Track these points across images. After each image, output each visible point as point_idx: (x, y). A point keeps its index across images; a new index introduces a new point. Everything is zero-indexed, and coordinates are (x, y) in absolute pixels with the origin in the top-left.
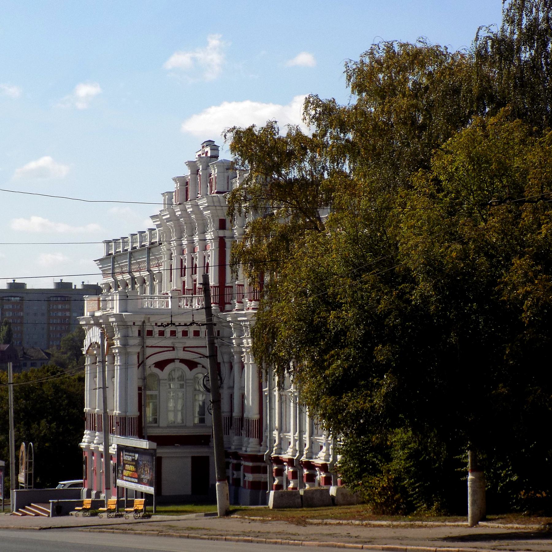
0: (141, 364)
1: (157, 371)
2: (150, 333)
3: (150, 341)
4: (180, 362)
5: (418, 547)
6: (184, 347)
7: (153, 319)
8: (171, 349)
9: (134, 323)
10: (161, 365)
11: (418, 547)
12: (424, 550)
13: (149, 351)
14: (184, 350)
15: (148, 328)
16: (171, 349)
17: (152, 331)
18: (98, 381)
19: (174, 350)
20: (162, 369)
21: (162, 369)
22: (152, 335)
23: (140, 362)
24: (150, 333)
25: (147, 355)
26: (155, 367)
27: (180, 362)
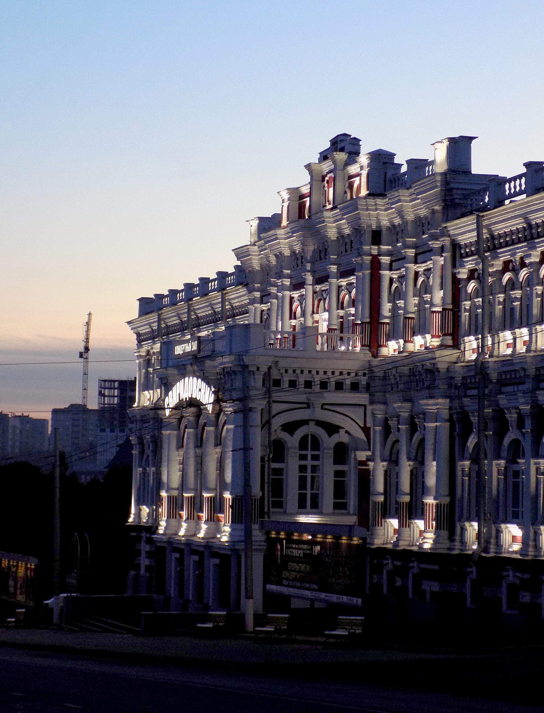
0: (266, 424)
1: (284, 436)
2: (277, 383)
3: (276, 395)
4: (316, 424)
5: (191, 582)
6: (323, 405)
7: (283, 363)
8: (325, 407)
9: (258, 368)
10: (290, 428)
11: (191, 582)
12: (280, 614)
13: (276, 408)
14: (322, 408)
15: (275, 375)
16: (325, 407)
17: (296, 381)
18: (393, 456)
19: (308, 407)
20: (292, 434)
21: (292, 434)
22: (326, 383)
23: (263, 422)
24: (277, 383)
25: (274, 412)
26: (282, 430)
27: (316, 424)
